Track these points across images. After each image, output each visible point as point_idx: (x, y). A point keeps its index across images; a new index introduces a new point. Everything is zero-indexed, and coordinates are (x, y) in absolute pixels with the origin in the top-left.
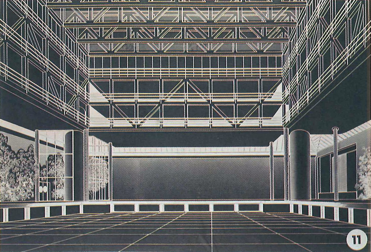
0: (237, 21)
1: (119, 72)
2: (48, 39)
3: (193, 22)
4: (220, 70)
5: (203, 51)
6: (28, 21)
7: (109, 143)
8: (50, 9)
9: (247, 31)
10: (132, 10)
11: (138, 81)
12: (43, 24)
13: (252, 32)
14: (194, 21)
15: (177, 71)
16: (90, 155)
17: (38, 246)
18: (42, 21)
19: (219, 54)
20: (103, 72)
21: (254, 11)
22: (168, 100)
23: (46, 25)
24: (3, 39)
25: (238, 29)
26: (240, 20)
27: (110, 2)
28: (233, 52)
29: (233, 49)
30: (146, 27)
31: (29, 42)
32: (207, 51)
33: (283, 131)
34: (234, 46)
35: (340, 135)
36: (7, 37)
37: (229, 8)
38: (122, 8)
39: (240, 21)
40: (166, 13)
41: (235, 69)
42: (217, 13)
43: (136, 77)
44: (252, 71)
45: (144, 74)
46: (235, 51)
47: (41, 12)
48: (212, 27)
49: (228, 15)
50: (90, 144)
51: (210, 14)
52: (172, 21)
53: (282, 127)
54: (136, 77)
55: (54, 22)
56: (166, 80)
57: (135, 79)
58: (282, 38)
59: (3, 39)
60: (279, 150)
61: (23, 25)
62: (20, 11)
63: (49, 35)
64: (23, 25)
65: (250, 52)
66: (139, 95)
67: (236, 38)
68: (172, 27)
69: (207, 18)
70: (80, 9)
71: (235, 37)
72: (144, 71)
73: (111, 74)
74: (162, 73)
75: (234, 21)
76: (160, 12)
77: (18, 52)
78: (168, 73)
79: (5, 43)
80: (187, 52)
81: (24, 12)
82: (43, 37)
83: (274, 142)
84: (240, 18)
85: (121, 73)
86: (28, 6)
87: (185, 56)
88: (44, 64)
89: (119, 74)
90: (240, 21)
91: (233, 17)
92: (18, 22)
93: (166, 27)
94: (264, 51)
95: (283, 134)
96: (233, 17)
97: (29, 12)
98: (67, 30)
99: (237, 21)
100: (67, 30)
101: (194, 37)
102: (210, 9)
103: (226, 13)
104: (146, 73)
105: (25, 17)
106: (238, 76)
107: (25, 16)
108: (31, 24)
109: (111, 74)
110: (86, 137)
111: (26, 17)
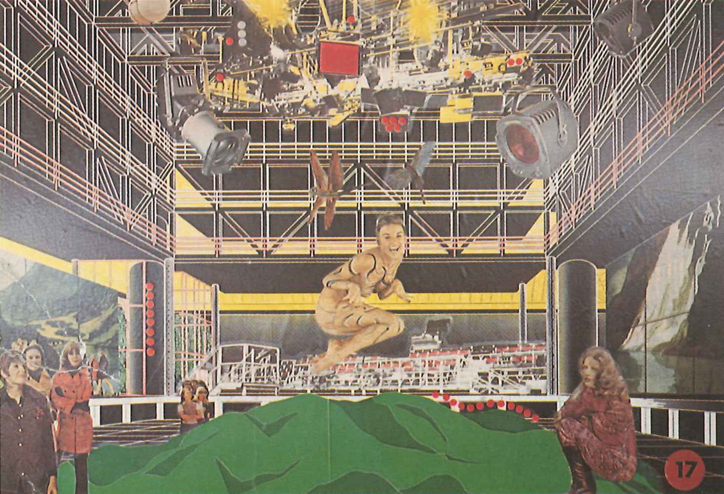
6: (60, 53)
37: (555, 26)
54: (454, 159)
56: (273, 166)
61: (50, 61)
63: (98, 79)
88: (89, 134)
89: (280, 155)
105: (54, 45)
108: (64, 58)
109: (454, 154)
111: (56, 46)
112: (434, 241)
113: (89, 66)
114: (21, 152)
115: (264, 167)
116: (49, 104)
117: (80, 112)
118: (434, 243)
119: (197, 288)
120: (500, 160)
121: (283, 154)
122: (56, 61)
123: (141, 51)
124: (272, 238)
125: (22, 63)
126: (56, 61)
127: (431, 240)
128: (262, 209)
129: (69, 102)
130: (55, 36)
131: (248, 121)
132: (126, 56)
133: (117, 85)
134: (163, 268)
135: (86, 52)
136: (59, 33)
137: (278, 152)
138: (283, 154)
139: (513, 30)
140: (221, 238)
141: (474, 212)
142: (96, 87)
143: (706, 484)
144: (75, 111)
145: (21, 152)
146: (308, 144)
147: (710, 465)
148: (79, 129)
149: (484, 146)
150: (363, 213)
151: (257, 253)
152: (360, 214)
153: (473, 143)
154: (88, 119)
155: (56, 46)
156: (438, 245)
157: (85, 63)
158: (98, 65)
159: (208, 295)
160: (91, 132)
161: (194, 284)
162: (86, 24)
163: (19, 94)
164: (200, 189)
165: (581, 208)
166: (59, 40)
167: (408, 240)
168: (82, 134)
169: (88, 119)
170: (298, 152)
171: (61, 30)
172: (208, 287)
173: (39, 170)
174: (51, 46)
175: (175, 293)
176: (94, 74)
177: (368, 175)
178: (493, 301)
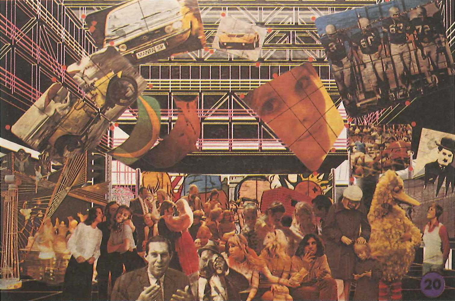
0: (292, 23)
1: (210, 83)
2: (64, 44)
3: (306, 24)
4: (241, 82)
5: (192, 59)
6: (41, 22)
7: (137, 169)
8: (68, 8)
9: (304, 35)
10: (238, 10)
11: (203, 95)
12: (59, 26)
13: (310, 37)
14: (307, 23)
15: (330, 84)
16: (114, 182)
17: (48, 294)
18: (58, 22)
19: (271, 62)
20: (190, 83)
21: (313, 11)
22: (209, 118)
23: (62, 27)
24: (10, 44)
25: (293, 33)
26: (296, 22)
27: (301, 1)
28: (288, 60)
29: (288, 57)
30: (313, 31)
31: (42, 46)
32: (197, 59)
33: (347, 156)
34: (288, 54)
35: (414, 160)
36: (15, 41)
37: (211, 7)
38: (227, 7)
39: (297, 24)
40: (207, 14)
41: (230, 80)
42: (269, 13)
43: (170, 90)
44: (240, 83)
45: (190, 87)
46: (290, 59)
47: (55, 11)
48: (295, 31)
49: (281, 16)
50: (114, 169)
51: (261, 15)
52: (279, 23)
53: (346, 151)
54: (200, 90)
55: (72, 24)
56: (206, 94)
57: (169, 92)
58: (288, 43)
59: (10, 44)
60: (342, 178)
61: (35, 27)
62: (31, 10)
63: (65, 39)
64: (35, 27)
65: (189, 60)
66: (228, 112)
67: (291, 43)
68: (279, 31)
69: (256, 19)
70: (249, 9)
71: (289, 43)
72: (180, 83)
73: (200, 87)
74: (232, 85)
75: (289, 23)
76: (272, 12)
77: (28, 60)
78: (239, 85)
79: (13, 50)
80: (233, 60)
81: (36, 12)
82: (58, 41)
83: (337, 168)
84: (297, 18)
85: (241, 85)
86: (41, 5)
87: (230, 65)
88: (59, 73)
89: (220, 87)
90: (297, 24)
91: (287, 19)
92: (28, 24)
93: (208, 31)
94: (265, 60)
95: (347, 159)
96: (287, 19)
97: (43, 12)
98: (88, 33)
99: (292, 23)
100: (88, 33)
101: (300, 42)
102: (296, 9)
103: (279, 14)
104: (182, 85)
105: (37, 18)
106: (234, 88)
107: (37, 16)
108: (44, 25)
109: (230, 87)
110: (109, 162)
111: (39, 18)
112: (277, 141)
113: (59, 31)
114: (16, 85)
115: (170, 94)
116: (33, 55)
117: (54, 60)
118: (278, 143)
119: (127, 170)
120: (199, 91)
121: (162, 87)
122: (39, 27)
123: (288, 22)
124: (264, 139)
125: (17, 29)
126: (39, 27)
127: (275, 141)
128: (168, 121)
129: (46, 53)
130: (38, 12)
131: (240, 66)
132: (83, 25)
133: (77, 43)
134: (105, 158)
135: (58, 22)
136: (41, 10)
137: (249, 85)
138: (162, 87)
139: (292, 9)
140: (262, 139)
141: (222, 123)
142: (64, 44)
143: (446, 294)
144: (50, 59)
145: (16, 85)
146: (327, 80)
147: (449, 283)
148: (52, 70)
149: (189, 82)
150: (233, 124)
151: (286, 149)
152: (231, 124)
153: (232, 80)
154: (58, 64)
155: (39, 18)
156: (280, 144)
157: (57, 29)
158: (65, 30)
159: (134, 174)
160: (60, 72)
161: (125, 168)
162: (58, 4)
163: (15, 48)
164: (249, 109)
165: (370, 121)
166: (41, 15)
167: (261, 141)
168: (54, 73)
169: (58, 64)
170: (232, 85)
171: (42, 8)
172: (133, 170)
173: (28, 97)
174: (36, 18)
175: (112, 174)
176: (62, 36)
177: (236, 100)
178: (340, 180)
